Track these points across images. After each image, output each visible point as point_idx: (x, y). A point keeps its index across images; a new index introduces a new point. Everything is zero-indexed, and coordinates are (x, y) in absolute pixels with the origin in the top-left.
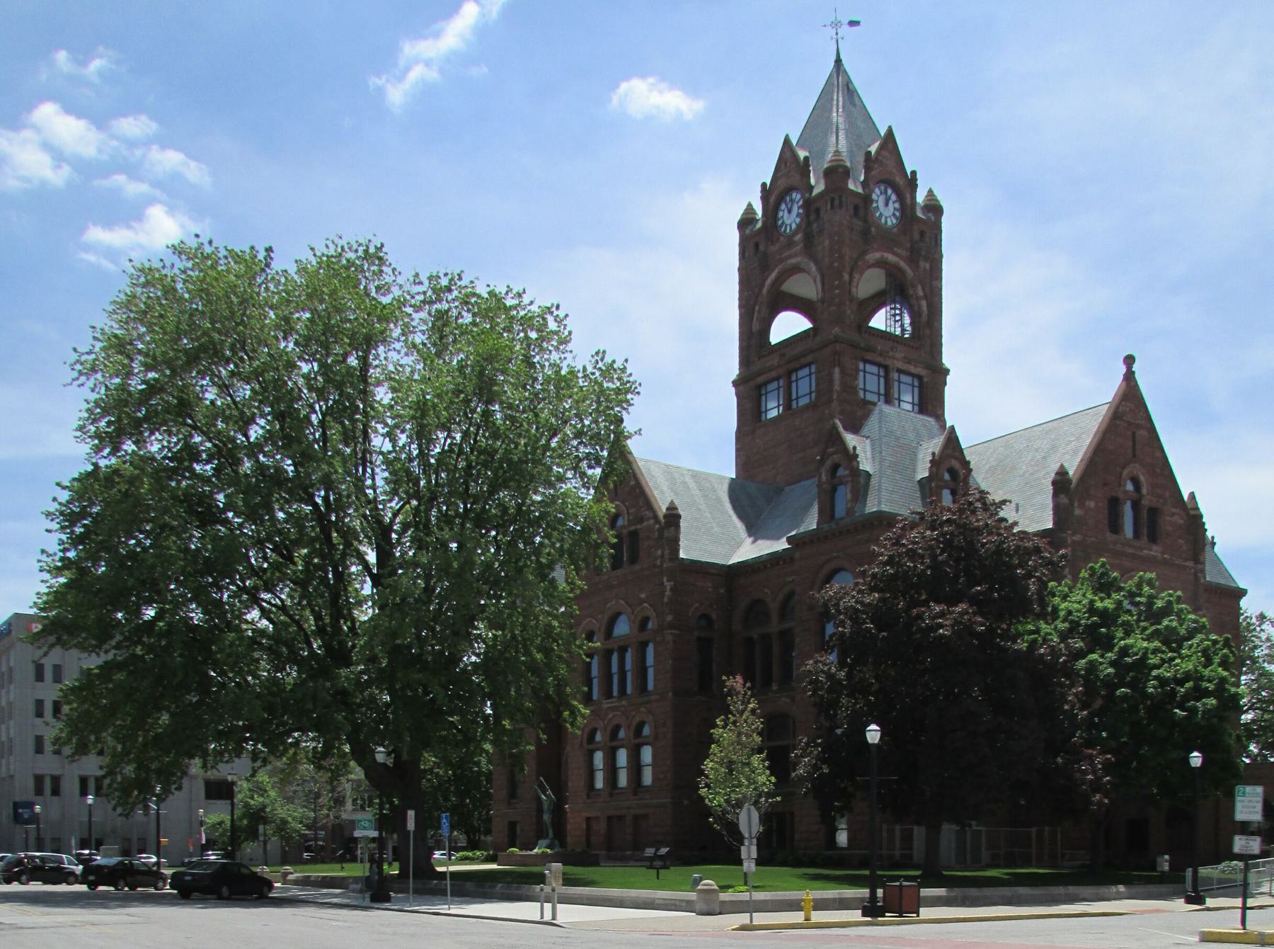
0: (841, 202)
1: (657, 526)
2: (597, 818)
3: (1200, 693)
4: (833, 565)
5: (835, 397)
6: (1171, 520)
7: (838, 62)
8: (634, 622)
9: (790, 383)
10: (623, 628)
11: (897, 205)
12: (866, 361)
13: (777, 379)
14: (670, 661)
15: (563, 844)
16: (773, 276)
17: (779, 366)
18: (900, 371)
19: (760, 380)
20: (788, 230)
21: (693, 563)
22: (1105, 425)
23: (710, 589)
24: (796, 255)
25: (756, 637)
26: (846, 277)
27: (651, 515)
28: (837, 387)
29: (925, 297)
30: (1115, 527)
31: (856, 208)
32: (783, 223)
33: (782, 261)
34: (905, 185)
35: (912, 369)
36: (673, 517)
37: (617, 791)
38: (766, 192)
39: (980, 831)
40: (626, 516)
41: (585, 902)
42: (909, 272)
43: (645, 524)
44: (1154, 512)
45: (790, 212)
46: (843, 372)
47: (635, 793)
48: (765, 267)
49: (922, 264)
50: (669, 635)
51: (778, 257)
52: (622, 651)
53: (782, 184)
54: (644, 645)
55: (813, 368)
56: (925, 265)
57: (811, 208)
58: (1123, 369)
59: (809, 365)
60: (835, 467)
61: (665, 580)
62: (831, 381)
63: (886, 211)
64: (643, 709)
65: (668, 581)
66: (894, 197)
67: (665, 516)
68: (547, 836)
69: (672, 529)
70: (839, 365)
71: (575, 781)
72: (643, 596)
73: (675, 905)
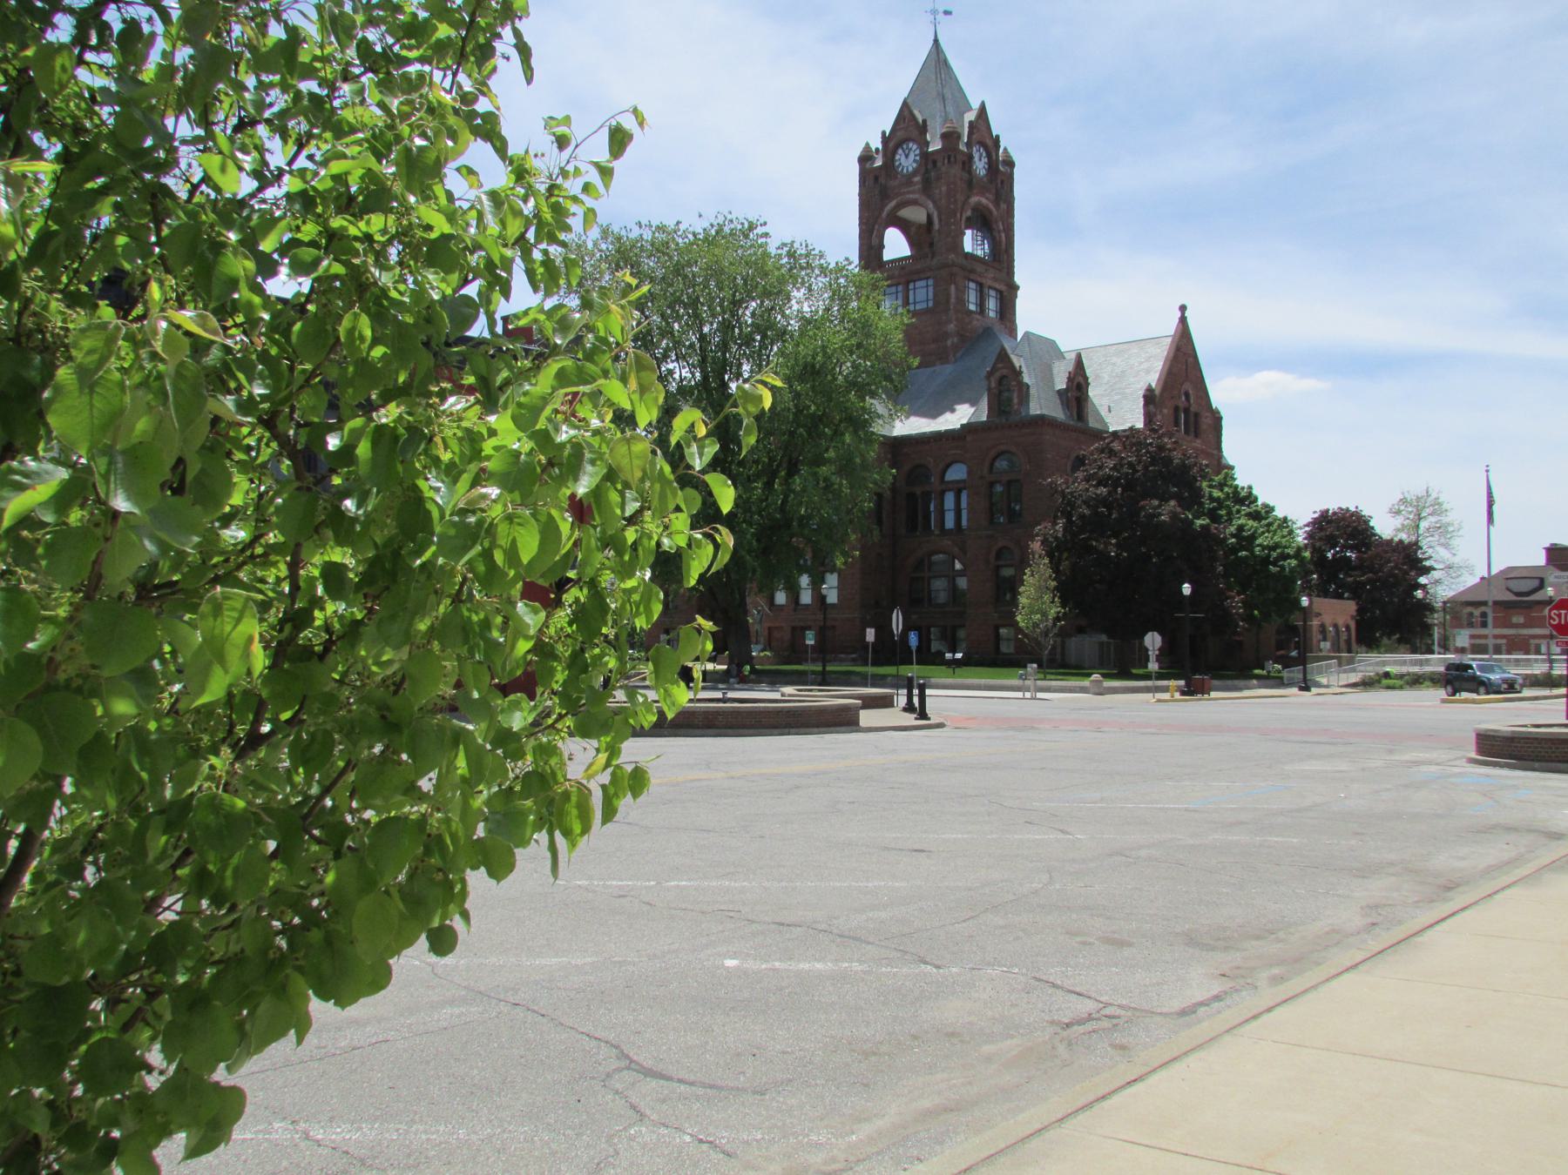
3: (1285, 557)
4: (1003, 448)
6: (1206, 421)
7: (936, 41)
9: (908, 290)
12: (970, 280)
16: (893, 203)
22: (1171, 355)
28: (953, 300)
30: (1177, 423)
31: (964, 163)
35: (997, 286)
38: (886, 140)
42: (995, 212)
44: (1197, 415)
45: (907, 156)
46: (957, 289)
53: (900, 134)
55: (931, 282)
56: (1003, 206)
59: (927, 278)
62: (948, 296)
63: (980, 166)
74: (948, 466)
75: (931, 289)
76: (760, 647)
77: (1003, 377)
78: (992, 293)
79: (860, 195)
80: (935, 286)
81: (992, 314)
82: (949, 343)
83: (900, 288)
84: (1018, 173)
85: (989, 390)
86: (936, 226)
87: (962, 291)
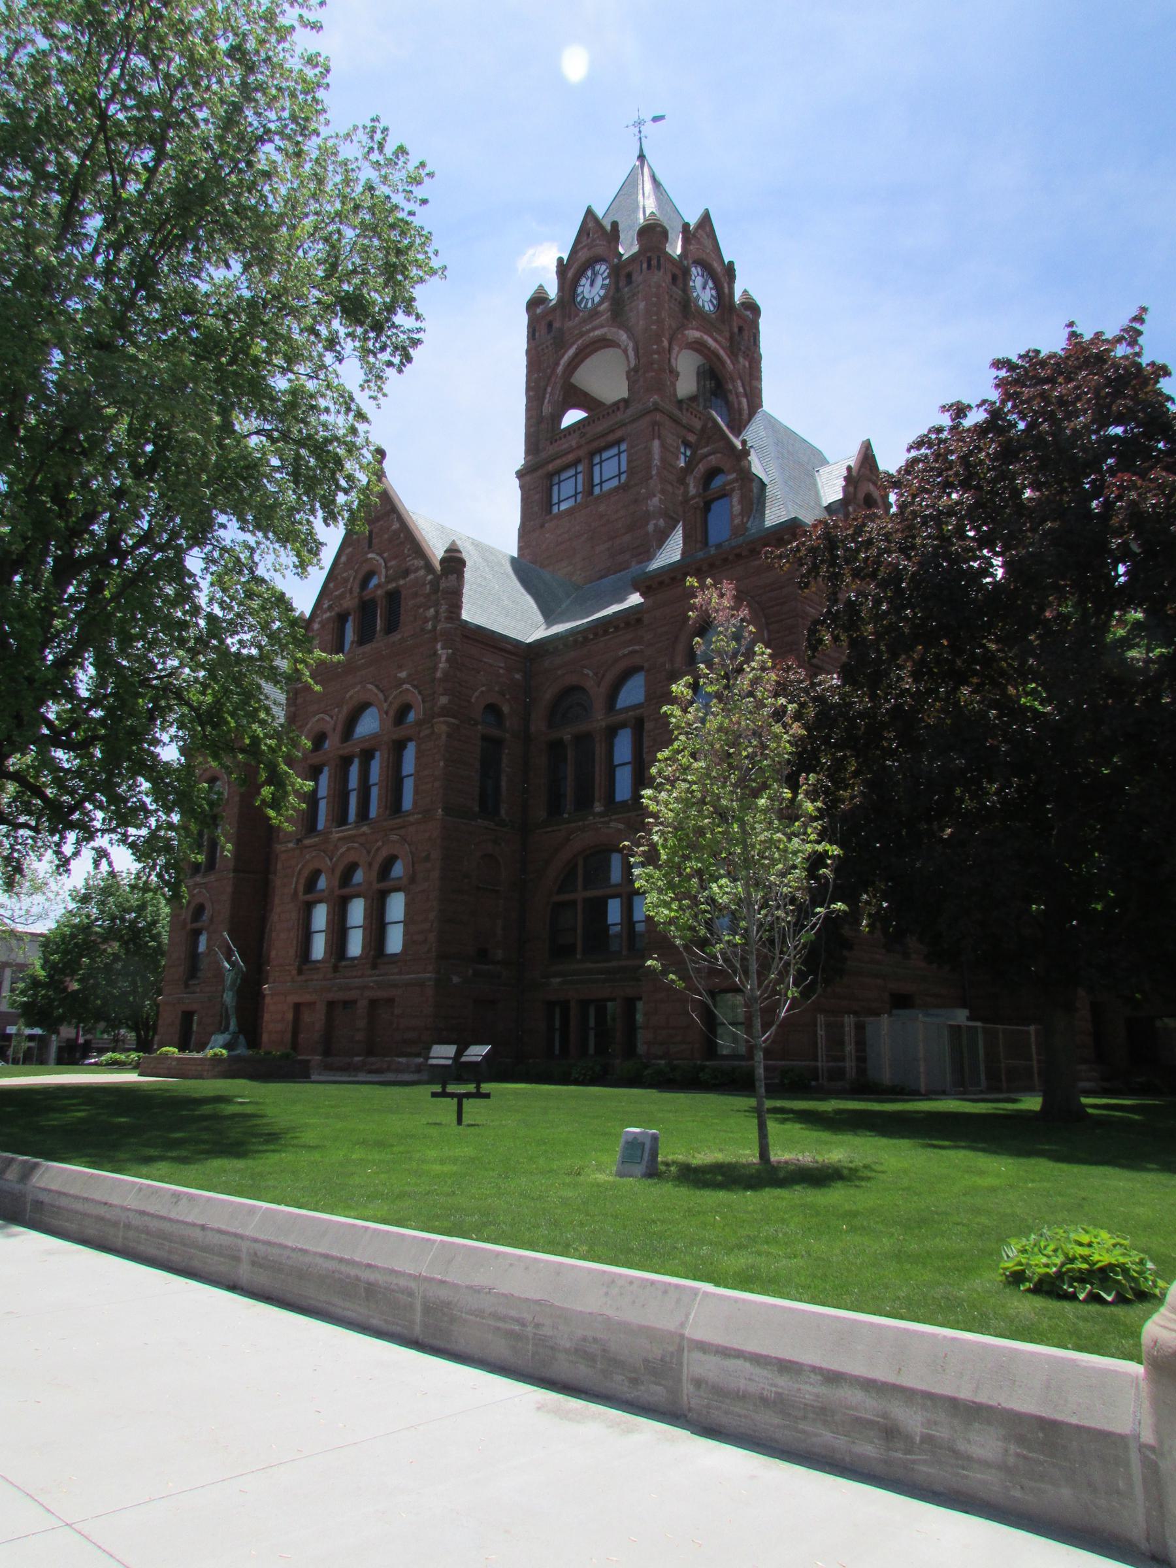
0: (659, 261)
1: (430, 577)
2: (311, 1004)
5: (654, 472)
8: (387, 713)
10: (369, 725)
11: (714, 292)
14: (442, 764)
15: (253, 1041)
17: (579, 447)
19: (550, 467)
20: (590, 305)
21: (479, 629)
23: (501, 671)
24: (602, 326)
25: (567, 737)
26: (666, 343)
27: (422, 563)
28: (656, 461)
29: (746, 395)
33: (582, 335)
34: (721, 276)
36: (454, 562)
37: (343, 963)
38: (562, 268)
39: (976, 1027)
40: (383, 571)
41: (244, 1272)
43: (412, 576)
45: (592, 285)
46: (663, 446)
47: (374, 966)
48: (560, 344)
49: (741, 360)
50: (441, 727)
51: (576, 332)
52: (367, 756)
53: (583, 255)
54: (399, 747)
55: (623, 447)
57: (622, 273)
59: (618, 443)
60: (712, 473)
61: (439, 646)
63: (704, 295)
64: (394, 837)
65: (443, 648)
66: (710, 284)
67: (443, 561)
68: (227, 1029)
69: (453, 577)
70: (659, 438)
71: (281, 947)
72: (403, 675)
73: (890, 1433)
75: (624, 457)
77: (712, 473)
79: (528, 352)
84: (766, 328)
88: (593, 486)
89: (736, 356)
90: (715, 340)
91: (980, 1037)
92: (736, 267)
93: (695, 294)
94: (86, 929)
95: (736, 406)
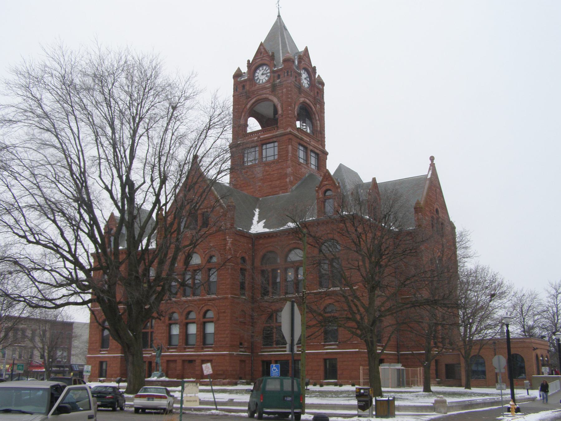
1: (222, 210)
5: (289, 159)
7: (279, 16)
9: (262, 150)
13: (255, 147)
18: (312, 151)
20: (261, 82)
29: (319, 120)
32: (258, 78)
34: (311, 71)
38: (249, 65)
53: (259, 61)
55: (276, 144)
58: (430, 162)
59: (274, 142)
62: (287, 151)
74: (290, 251)
75: (276, 148)
76: (158, 373)
78: (313, 154)
80: (278, 146)
81: (313, 167)
82: (288, 180)
83: (257, 149)
85: (318, 199)
86: (280, 112)
87: (295, 150)
88: (262, 158)
89: (316, 105)
90: (309, 100)
91: (405, 371)
92: (316, 69)
93: (302, 82)
94: (400, 384)
95: (316, 125)
